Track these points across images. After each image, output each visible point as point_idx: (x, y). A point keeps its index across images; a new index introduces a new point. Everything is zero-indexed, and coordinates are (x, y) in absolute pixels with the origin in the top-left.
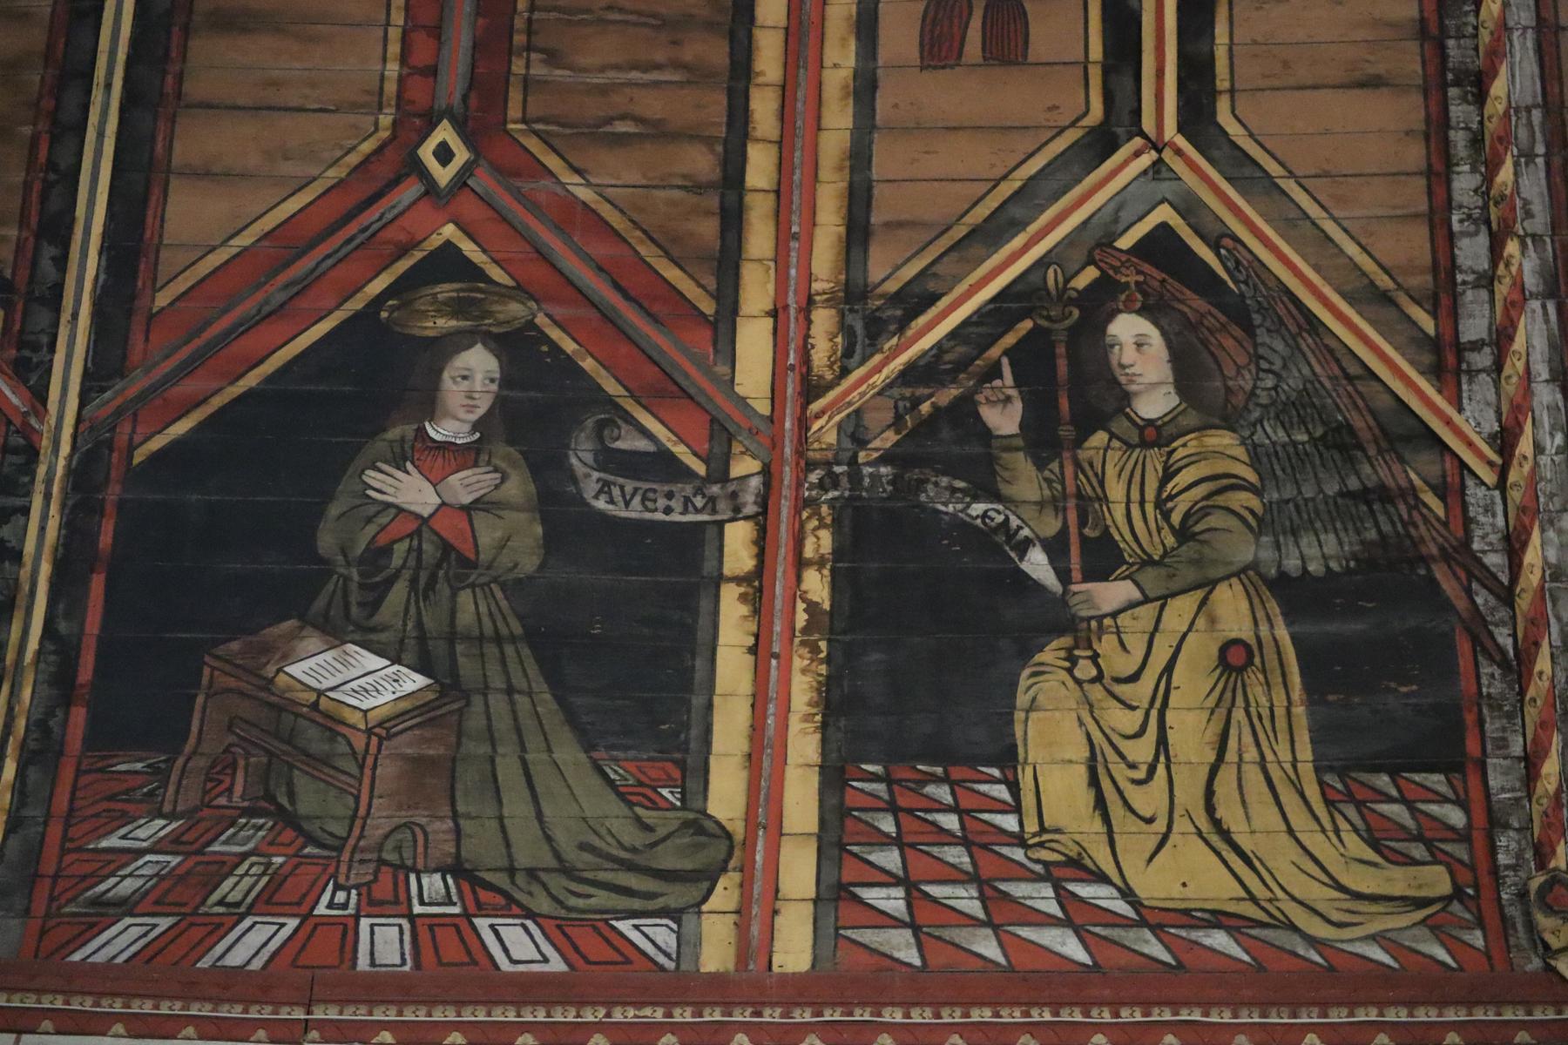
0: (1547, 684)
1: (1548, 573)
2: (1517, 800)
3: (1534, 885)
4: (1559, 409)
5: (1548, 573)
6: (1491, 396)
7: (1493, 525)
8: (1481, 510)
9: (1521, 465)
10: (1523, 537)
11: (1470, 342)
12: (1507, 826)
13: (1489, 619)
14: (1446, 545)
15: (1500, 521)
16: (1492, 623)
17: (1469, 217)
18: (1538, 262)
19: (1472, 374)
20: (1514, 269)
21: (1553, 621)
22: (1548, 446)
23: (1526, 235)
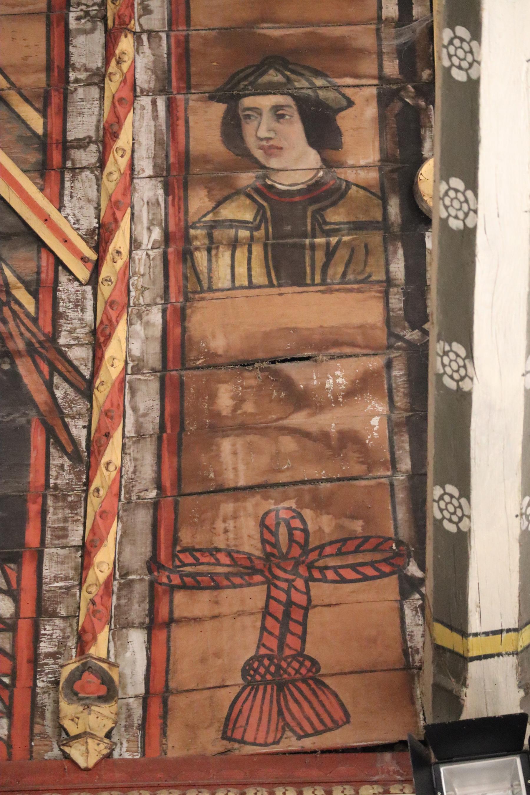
0: (113, 474)
1: (131, 364)
2: (68, 588)
3: (66, 672)
4: (158, 204)
5: (131, 364)
6: (93, 194)
7: (81, 320)
8: (71, 305)
9: (114, 262)
10: (107, 331)
11: (76, 140)
12: (54, 615)
13: (66, 412)
14: (34, 341)
15: (89, 316)
16: (68, 416)
17: (87, 13)
18: (152, 58)
19: (76, 171)
20: (125, 67)
21: (129, 411)
22: (145, 241)
23: (143, 31)
